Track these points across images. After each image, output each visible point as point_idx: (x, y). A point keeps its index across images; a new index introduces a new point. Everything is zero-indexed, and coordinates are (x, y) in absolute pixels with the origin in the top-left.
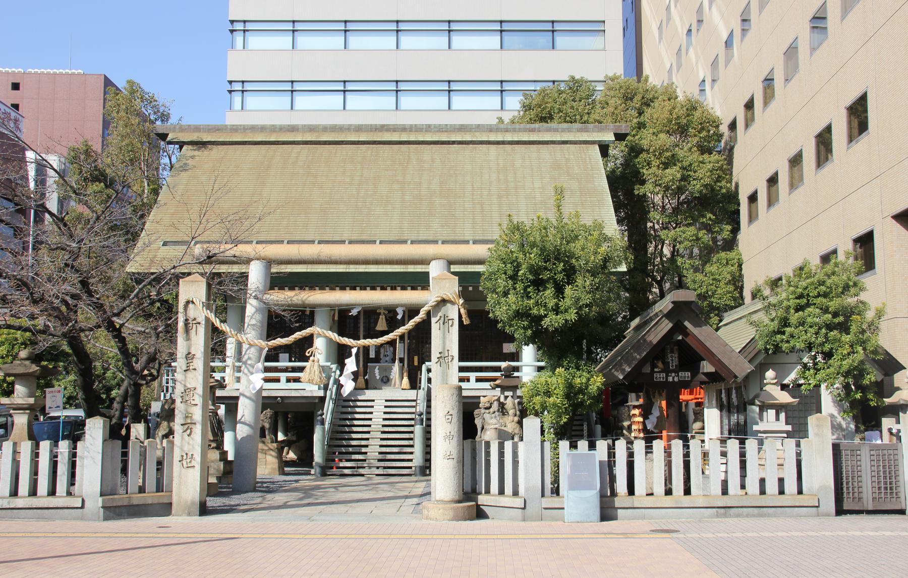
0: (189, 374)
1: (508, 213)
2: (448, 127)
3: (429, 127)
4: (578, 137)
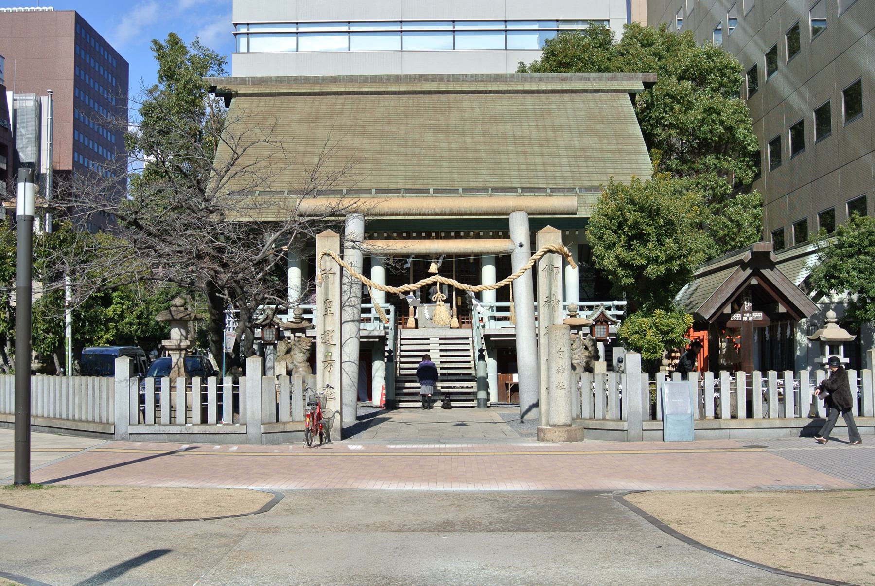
0: (329, 318)
1: (611, 175)
2: (484, 76)
3: (466, 77)
4: (609, 86)
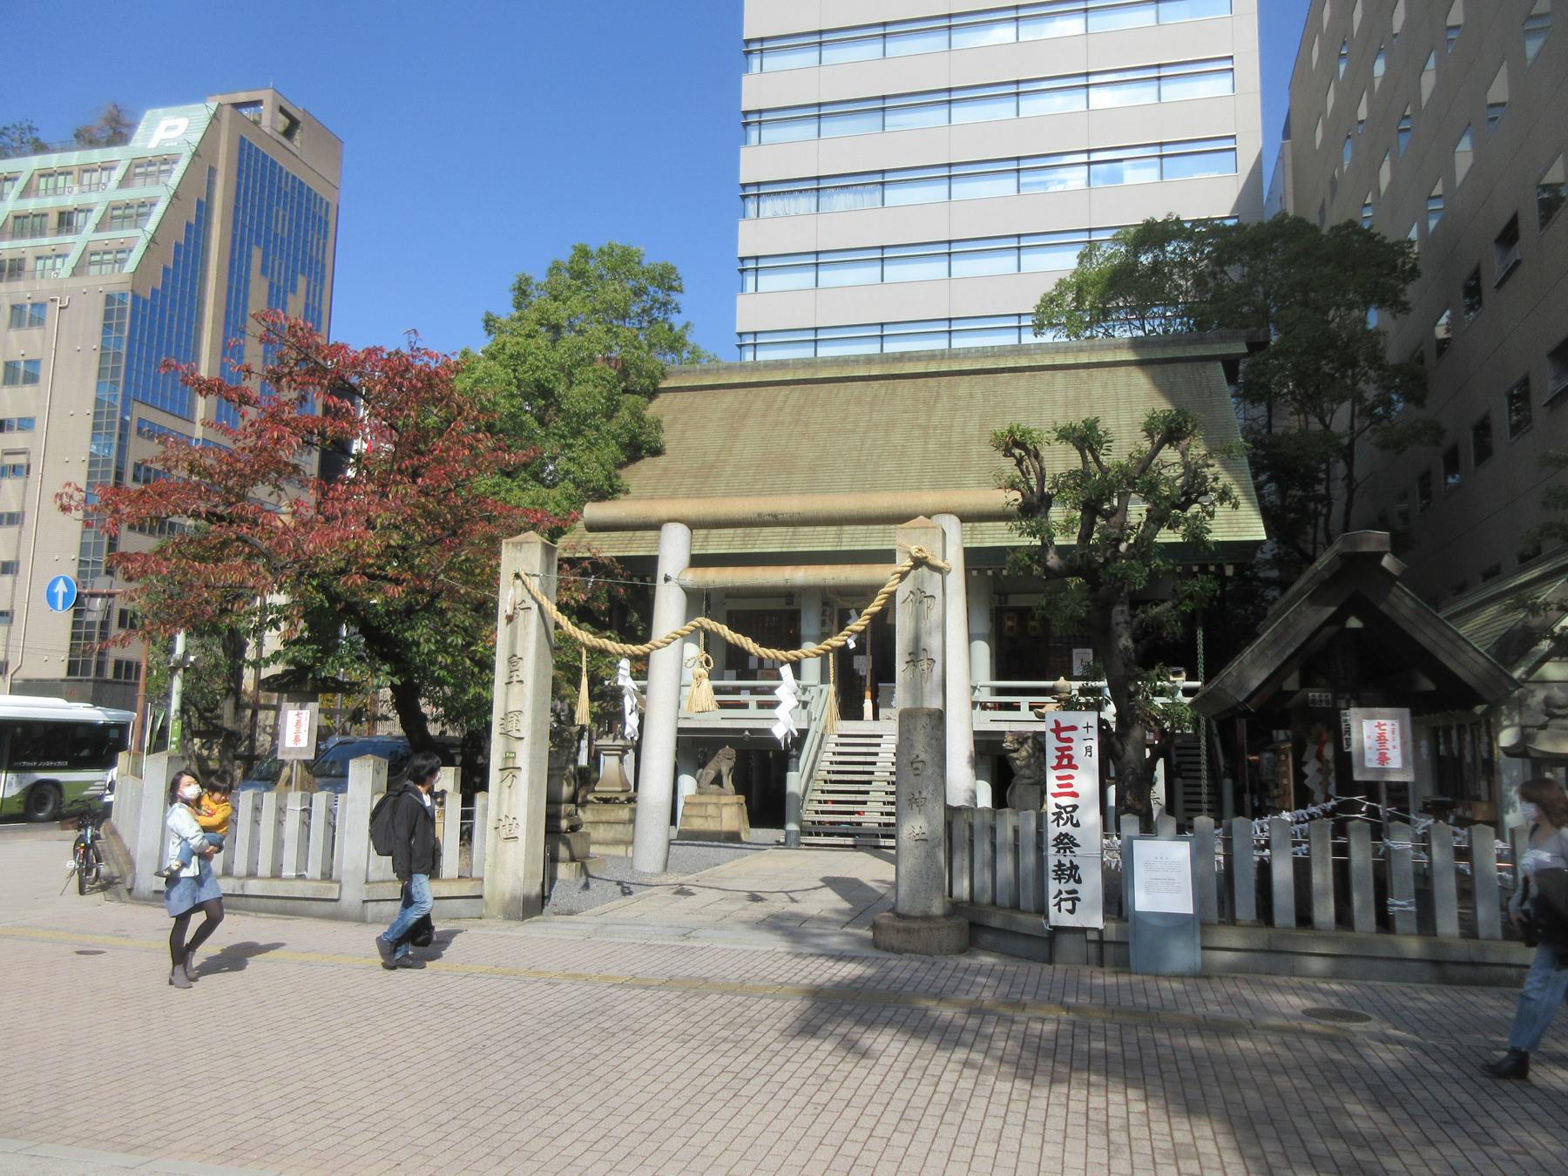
0: (515, 688)
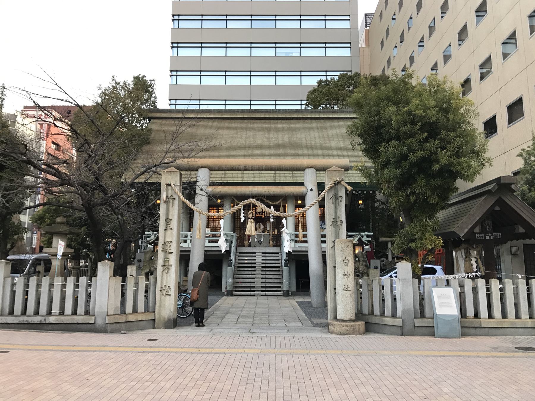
0: (169, 232)
